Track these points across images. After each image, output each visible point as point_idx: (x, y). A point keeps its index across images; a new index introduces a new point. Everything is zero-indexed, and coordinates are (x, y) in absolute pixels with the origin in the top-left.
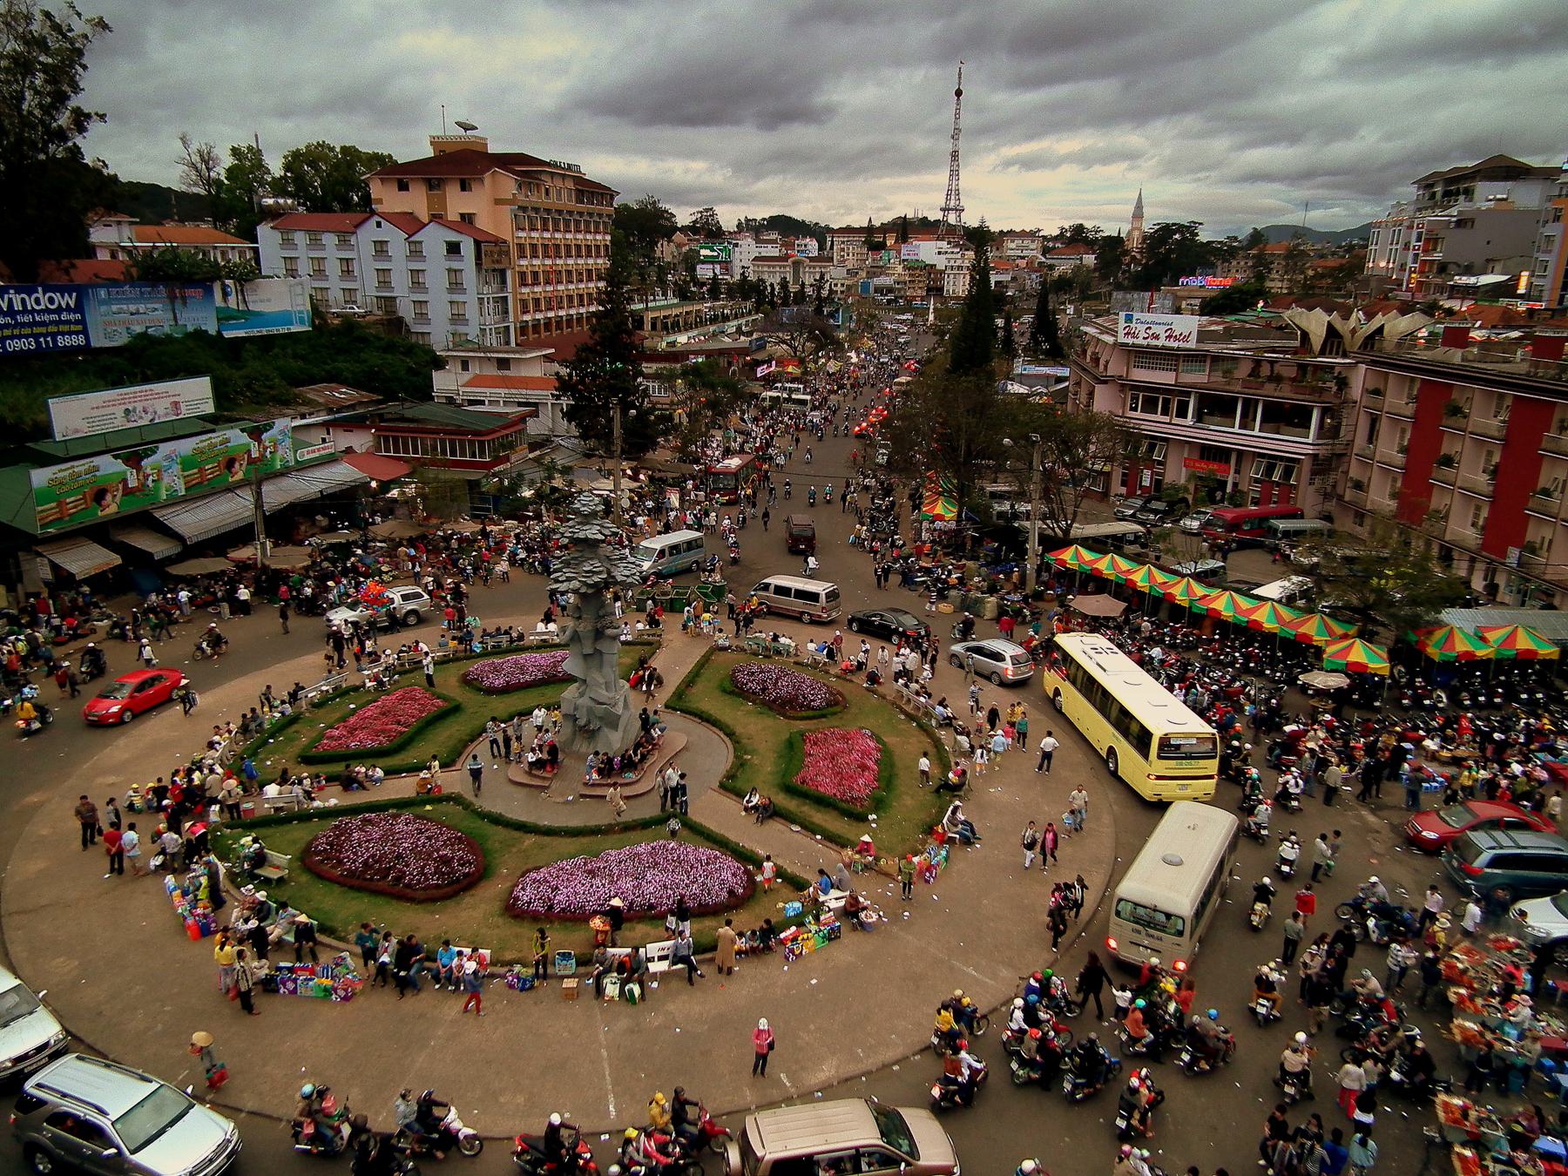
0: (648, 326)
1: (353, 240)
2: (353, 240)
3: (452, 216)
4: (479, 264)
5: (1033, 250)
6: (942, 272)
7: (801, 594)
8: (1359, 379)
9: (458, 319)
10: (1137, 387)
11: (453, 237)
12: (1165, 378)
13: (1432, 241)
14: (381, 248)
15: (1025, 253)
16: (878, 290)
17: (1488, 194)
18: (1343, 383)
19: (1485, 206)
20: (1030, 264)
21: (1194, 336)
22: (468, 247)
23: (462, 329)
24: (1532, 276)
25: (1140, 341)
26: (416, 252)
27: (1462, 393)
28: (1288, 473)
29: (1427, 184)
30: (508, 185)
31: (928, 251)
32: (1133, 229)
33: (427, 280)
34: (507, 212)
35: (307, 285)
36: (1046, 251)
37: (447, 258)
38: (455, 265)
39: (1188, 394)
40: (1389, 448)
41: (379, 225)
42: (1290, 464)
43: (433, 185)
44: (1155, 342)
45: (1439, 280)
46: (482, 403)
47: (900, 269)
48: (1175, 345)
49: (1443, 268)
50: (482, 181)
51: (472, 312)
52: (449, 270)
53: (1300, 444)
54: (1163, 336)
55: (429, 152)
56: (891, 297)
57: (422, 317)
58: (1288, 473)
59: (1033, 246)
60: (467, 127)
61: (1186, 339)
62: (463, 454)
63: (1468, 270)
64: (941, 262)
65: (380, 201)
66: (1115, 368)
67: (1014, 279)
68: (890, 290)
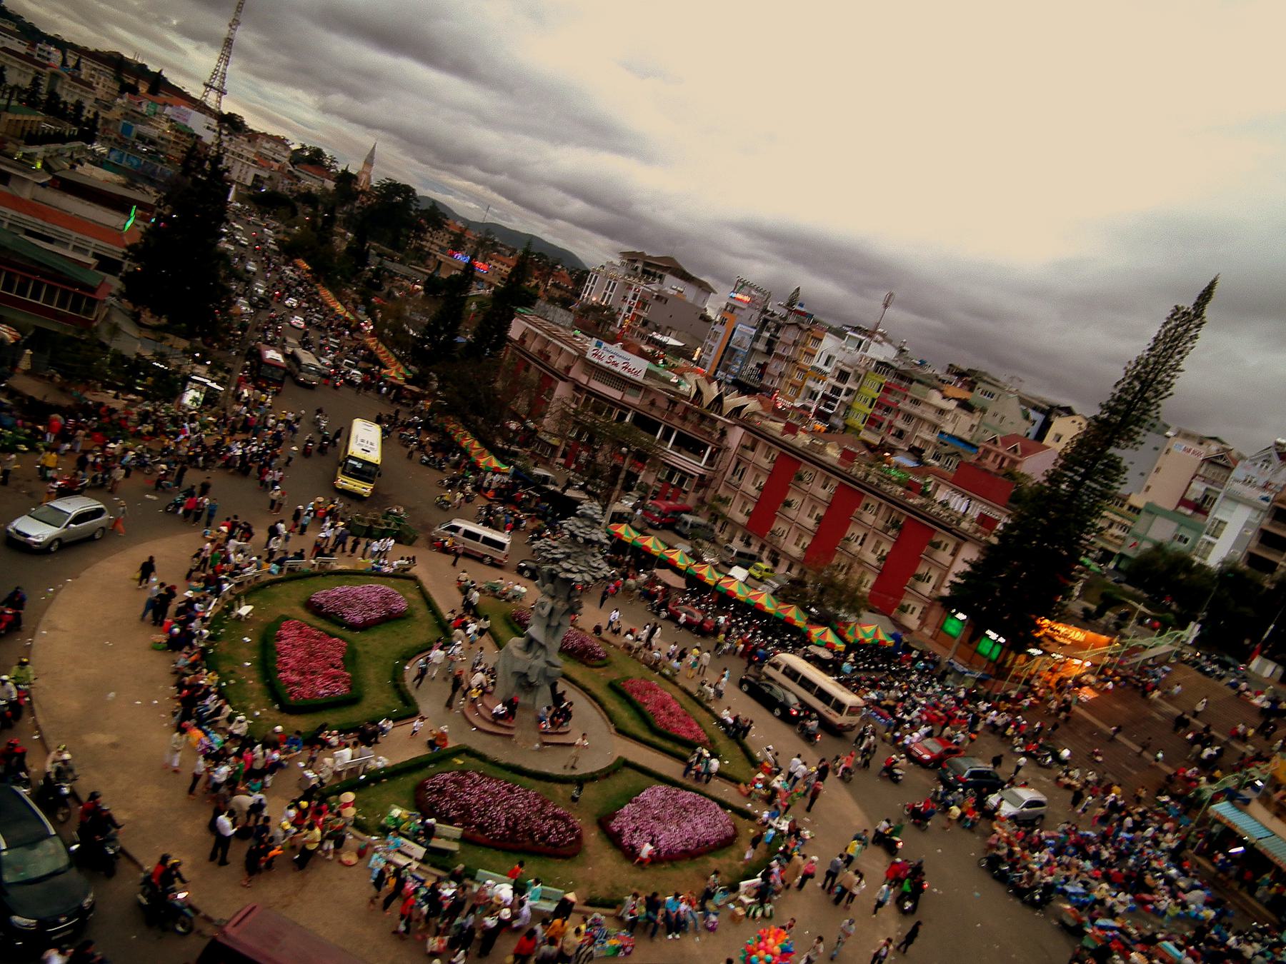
7: (487, 541)
8: (736, 436)
10: (592, 393)
12: (616, 394)
13: (643, 304)
15: (276, 157)
16: (141, 137)
17: (671, 285)
18: (723, 433)
19: (671, 292)
20: (281, 168)
21: (642, 374)
24: (702, 351)
25: (603, 363)
27: (806, 469)
28: (681, 481)
29: (631, 258)
31: (199, 124)
39: (628, 410)
40: (750, 486)
42: (685, 475)
44: (613, 367)
45: (643, 331)
46: (50, 240)
48: (628, 375)
49: (645, 323)
53: (695, 465)
54: (621, 366)
56: (151, 148)
58: (681, 481)
60: (1158, 470)
61: (636, 373)
62: (35, 296)
63: (657, 329)
66: (577, 373)
67: (270, 178)
68: (152, 142)
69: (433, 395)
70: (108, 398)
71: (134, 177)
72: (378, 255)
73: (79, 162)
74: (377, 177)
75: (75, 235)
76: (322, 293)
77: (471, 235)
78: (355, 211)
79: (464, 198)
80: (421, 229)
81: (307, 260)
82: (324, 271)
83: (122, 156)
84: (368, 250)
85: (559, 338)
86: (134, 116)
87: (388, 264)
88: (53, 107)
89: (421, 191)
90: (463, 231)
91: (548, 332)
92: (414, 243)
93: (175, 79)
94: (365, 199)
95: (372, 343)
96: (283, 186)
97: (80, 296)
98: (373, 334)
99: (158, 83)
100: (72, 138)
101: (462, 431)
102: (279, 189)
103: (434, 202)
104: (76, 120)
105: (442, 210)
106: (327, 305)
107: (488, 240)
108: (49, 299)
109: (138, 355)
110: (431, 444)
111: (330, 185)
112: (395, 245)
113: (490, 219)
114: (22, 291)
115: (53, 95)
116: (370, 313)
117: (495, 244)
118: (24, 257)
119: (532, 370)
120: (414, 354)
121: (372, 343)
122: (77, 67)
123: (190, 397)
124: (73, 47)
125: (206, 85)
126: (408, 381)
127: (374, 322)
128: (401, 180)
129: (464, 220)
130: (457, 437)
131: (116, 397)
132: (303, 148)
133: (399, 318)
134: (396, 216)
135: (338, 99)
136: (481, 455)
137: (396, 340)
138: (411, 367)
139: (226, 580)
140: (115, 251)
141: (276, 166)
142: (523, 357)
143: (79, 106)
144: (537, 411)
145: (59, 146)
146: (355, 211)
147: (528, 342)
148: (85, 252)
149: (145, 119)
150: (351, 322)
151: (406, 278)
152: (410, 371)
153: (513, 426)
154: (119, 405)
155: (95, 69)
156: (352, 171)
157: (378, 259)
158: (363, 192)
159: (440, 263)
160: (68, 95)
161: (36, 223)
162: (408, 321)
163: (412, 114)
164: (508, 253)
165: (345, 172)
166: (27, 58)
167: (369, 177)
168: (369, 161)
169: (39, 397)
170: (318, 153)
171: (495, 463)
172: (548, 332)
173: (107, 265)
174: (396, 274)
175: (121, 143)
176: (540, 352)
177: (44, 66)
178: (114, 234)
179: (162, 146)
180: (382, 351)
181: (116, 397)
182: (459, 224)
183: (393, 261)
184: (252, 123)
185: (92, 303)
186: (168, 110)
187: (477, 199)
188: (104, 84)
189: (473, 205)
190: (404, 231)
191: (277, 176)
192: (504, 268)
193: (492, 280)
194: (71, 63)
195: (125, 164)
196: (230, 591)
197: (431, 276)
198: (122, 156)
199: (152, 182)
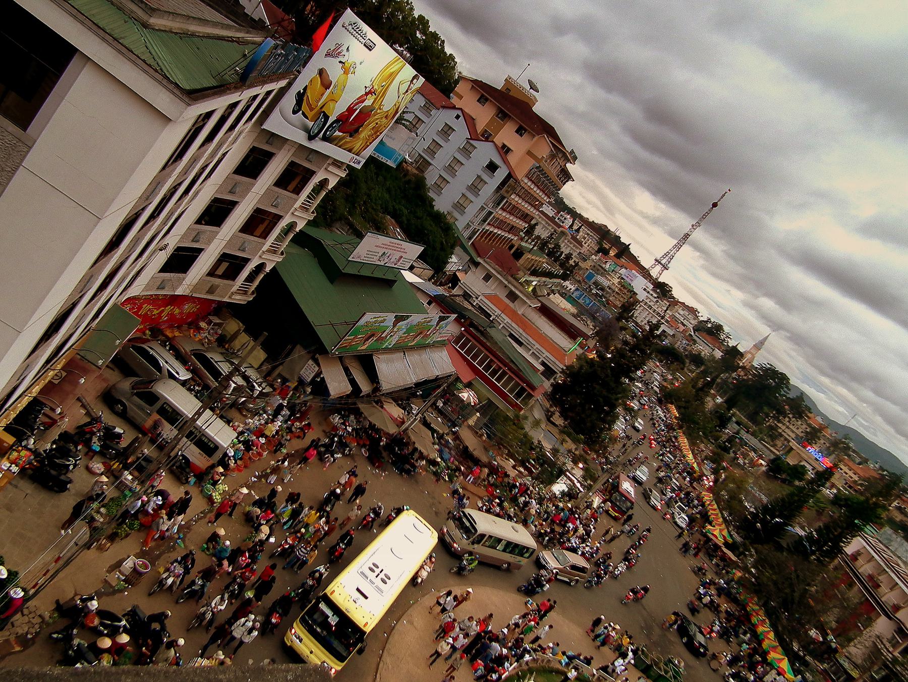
0: (521, 261)
1: (433, 112)
2: (433, 112)
3: (499, 139)
4: (499, 188)
5: (691, 324)
6: (638, 301)
9: (459, 207)
11: (498, 161)
14: (447, 131)
15: (685, 322)
16: (596, 284)
22: (501, 174)
23: (456, 214)
26: (466, 151)
30: (543, 149)
31: (640, 285)
32: (749, 352)
33: (460, 171)
34: (531, 163)
35: (422, 147)
36: (696, 329)
37: (483, 170)
38: (485, 177)
41: (458, 117)
43: (503, 115)
46: (520, 344)
47: (616, 281)
50: (534, 136)
51: (472, 210)
52: (478, 177)
55: (499, 85)
56: (600, 292)
57: (438, 188)
59: (693, 322)
60: (533, 87)
62: (498, 380)
64: (641, 296)
65: (460, 97)
68: (602, 289)
69: (746, 569)
70: (508, 465)
71: (582, 312)
72: (738, 423)
73: (553, 292)
74: (760, 360)
75: (537, 346)
76: (680, 439)
77: (828, 433)
78: (730, 380)
79: (832, 402)
80: (781, 412)
81: (678, 408)
82: (690, 422)
83: (581, 296)
84: (730, 418)
85: (897, 573)
86: (598, 269)
87: (744, 435)
88: (554, 254)
89: (793, 381)
90: (822, 428)
91: (887, 561)
92: (771, 422)
93: (634, 250)
94: (742, 373)
95: (707, 497)
96: (681, 345)
97: (525, 391)
98: (710, 489)
99: (624, 251)
100: (556, 276)
101: (762, 616)
102: (676, 346)
103: (802, 393)
104: (562, 265)
105: (806, 403)
106: (681, 450)
107: (844, 444)
108: (505, 386)
109: (539, 442)
110: (727, 612)
111: (718, 354)
112: (753, 417)
113: (853, 425)
114: (474, 357)
115: (557, 246)
116: (715, 472)
117: (849, 448)
118: (504, 353)
119: (855, 589)
120: (744, 524)
121: (707, 497)
122: (578, 231)
123: (559, 487)
124: (580, 217)
125: (656, 260)
126: (726, 544)
127: (716, 481)
128: (780, 368)
129: (825, 417)
130: (754, 620)
131: (514, 467)
132: (709, 321)
133: (740, 486)
134: (765, 395)
135: (767, 304)
136: (774, 648)
137: (731, 505)
138: (735, 535)
139: (529, 652)
140: (558, 366)
141: (682, 328)
142: (850, 577)
143: (569, 257)
144: (846, 632)
145: (548, 279)
146: (730, 380)
147: (861, 561)
148: (537, 358)
149: (604, 273)
150: (695, 472)
151: (755, 451)
152: (731, 536)
153: (813, 633)
154: (512, 473)
155: (588, 234)
156: (741, 349)
157: (736, 427)
158: (743, 368)
159: (792, 449)
160: (566, 248)
161: (518, 331)
162: (748, 493)
163: (832, 334)
164: (858, 460)
165: (734, 349)
166: (552, 219)
167: (753, 358)
168: (759, 346)
169: (471, 449)
170: (719, 328)
171: (785, 665)
172: (887, 561)
173: (549, 372)
174: (746, 444)
175: (585, 285)
176: (871, 577)
177: (559, 226)
178: (558, 352)
179: (608, 293)
180: (713, 510)
181: (514, 467)
182: (819, 419)
183: (748, 432)
184: (678, 293)
185: (530, 396)
186: (623, 271)
187: (844, 402)
188: (589, 243)
189: (841, 409)
190: (766, 409)
191: (680, 336)
192: (851, 473)
193: (837, 483)
194: (575, 227)
195: (581, 301)
196: (527, 663)
197: (778, 458)
198: (581, 296)
199: (594, 318)
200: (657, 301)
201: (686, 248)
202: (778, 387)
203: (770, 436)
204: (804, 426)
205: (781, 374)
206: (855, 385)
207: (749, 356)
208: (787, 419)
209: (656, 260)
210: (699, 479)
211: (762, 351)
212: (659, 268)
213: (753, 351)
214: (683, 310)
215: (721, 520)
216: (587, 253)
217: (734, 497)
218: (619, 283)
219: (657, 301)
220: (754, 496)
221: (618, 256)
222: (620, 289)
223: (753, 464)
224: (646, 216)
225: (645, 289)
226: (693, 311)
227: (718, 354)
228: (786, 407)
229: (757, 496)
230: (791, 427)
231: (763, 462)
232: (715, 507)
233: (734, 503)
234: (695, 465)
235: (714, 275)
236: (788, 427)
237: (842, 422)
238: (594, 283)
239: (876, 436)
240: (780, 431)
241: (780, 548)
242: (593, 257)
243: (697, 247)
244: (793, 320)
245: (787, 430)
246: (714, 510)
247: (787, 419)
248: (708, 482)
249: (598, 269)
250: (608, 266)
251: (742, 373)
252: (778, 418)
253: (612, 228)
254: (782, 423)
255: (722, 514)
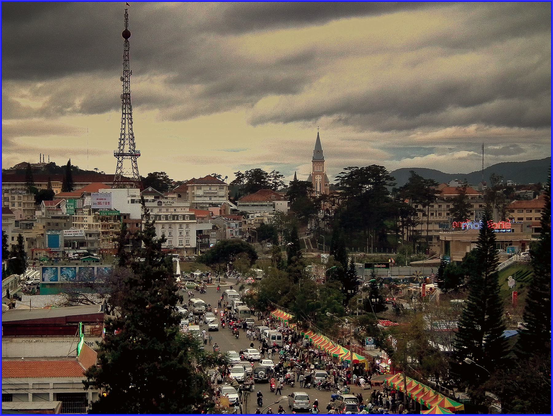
15: (214, 200)
16: (69, 243)
31: (123, 201)
32: (315, 174)
47: (90, 220)
56: (83, 250)
64: (136, 212)
68: (82, 244)
75: (31, 381)
76: (315, 342)
77: (474, 192)
80: (407, 212)
81: (286, 307)
82: (309, 314)
84: (353, 266)
87: (383, 272)
89: (391, 165)
90: (462, 192)
93: (84, 164)
95: (397, 381)
96: (232, 231)
99: (70, 176)
102: (229, 237)
103: (412, 171)
106: (326, 354)
112: (384, 245)
113: (490, 160)
117: (510, 189)
121: (397, 381)
125: (117, 155)
127: (390, 353)
128: (363, 162)
132: (240, 176)
133: (420, 336)
135: (270, 103)
140: (74, 383)
141: (216, 211)
149: (67, 221)
150: (363, 365)
151: (412, 280)
152: (458, 400)
156: (303, 177)
157: (369, 271)
158: (324, 197)
159: (447, 243)
162: (432, 334)
164: (530, 193)
165: (296, 184)
168: (318, 157)
170: (258, 175)
179: (92, 243)
183: (387, 266)
184: (176, 175)
186: (88, 201)
190: (388, 223)
191: (223, 222)
195: (61, 279)
197: (442, 265)
199: (91, 287)
200: (160, 203)
201: (135, 111)
202: (379, 185)
203: (419, 249)
204: (444, 206)
205: (369, 168)
206: (442, 115)
207: (318, 178)
208: (420, 214)
209: (117, 155)
210: (374, 369)
211: (327, 161)
212: (127, 163)
213: (318, 169)
214: (199, 188)
215: (432, 393)
216: (25, 216)
217: (424, 352)
218: (96, 219)
219: (160, 203)
220: (441, 332)
221: (67, 187)
222: (104, 226)
223: (422, 298)
224: (43, 112)
225: (133, 201)
226: (212, 180)
227: (283, 206)
228: (407, 201)
229: (442, 327)
230: (431, 219)
231: (432, 286)
232: (415, 383)
233: (430, 360)
234: (355, 357)
235: (177, 118)
236: (428, 223)
237: (476, 167)
238: (66, 245)
239: (520, 151)
240: (424, 234)
241: (510, 363)
242: (38, 213)
243: (150, 101)
244: (309, 97)
245: (431, 227)
246: (416, 388)
247: (420, 214)
248: (385, 365)
249: (57, 223)
250: (64, 209)
251: (328, 205)
252: (409, 221)
253: (34, 160)
254: (419, 223)
255: (428, 384)
